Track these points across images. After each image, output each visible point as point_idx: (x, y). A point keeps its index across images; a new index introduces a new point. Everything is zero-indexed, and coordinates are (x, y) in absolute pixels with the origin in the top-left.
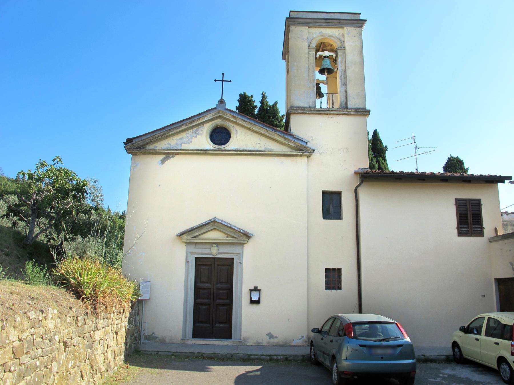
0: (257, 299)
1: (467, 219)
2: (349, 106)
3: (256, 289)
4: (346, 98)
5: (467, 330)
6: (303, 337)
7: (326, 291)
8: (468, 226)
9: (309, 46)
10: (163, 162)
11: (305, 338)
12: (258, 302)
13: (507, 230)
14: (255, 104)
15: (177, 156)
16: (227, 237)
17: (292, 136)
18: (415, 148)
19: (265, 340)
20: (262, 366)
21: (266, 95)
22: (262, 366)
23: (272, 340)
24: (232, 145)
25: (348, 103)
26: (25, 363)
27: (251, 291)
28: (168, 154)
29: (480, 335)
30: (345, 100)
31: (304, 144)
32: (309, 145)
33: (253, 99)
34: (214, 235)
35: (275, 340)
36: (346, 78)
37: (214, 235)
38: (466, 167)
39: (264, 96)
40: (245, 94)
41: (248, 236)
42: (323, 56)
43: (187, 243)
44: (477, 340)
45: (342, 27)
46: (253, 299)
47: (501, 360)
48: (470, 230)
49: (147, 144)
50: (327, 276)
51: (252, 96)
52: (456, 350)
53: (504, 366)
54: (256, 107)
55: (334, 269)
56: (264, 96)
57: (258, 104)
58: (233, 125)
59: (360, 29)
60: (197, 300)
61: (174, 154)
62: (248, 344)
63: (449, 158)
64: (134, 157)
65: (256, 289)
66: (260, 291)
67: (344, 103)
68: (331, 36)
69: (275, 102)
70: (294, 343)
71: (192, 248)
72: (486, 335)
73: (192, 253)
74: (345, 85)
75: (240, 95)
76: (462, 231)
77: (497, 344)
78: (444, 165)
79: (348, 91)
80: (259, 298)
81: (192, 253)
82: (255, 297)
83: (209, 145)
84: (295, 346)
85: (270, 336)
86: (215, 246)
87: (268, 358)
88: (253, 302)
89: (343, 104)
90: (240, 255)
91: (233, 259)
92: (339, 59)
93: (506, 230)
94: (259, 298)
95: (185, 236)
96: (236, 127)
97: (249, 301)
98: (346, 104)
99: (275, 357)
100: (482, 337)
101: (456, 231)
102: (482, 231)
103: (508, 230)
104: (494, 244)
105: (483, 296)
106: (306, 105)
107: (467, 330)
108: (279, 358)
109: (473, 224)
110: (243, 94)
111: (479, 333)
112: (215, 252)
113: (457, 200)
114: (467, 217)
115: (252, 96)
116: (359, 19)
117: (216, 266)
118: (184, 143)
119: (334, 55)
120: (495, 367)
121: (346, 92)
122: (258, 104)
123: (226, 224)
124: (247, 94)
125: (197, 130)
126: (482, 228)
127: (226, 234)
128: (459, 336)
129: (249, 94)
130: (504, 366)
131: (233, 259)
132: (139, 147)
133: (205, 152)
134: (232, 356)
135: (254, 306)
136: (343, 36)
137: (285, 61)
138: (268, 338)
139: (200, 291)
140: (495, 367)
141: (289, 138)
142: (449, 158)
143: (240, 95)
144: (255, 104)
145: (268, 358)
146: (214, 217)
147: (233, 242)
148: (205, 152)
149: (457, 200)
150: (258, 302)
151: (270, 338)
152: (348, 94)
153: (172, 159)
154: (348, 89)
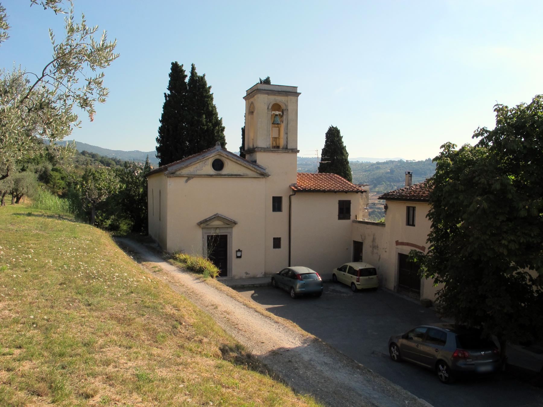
0: (240, 255)
2: (289, 147)
3: (239, 251)
4: (287, 142)
5: (340, 269)
6: (262, 273)
7: (275, 249)
9: (268, 108)
10: (187, 181)
11: (263, 273)
12: (240, 257)
14: (185, 74)
15: (194, 178)
16: (224, 224)
17: (258, 166)
18: (317, 150)
19: (244, 276)
21: (195, 66)
23: (247, 275)
24: (225, 171)
25: (288, 145)
27: (237, 251)
28: (189, 177)
29: (345, 272)
30: (286, 143)
31: (264, 171)
32: (267, 171)
33: (184, 68)
34: (217, 223)
35: (249, 275)
36: (287, 129)
37: (217, 223)
38: (341, 135)
39: (193, 68)
40: (176, 62)
41: (235, 223)
43: (202, 228)
44: (344, 274)
45: (287, 96)
46: (238, 255)
47: (353, 283)
49: (177, 171)
50: (274, 242)
51: (182, 65)
52: (335, 277)
53: (353, 286)
54: (186, 76)
55: (277, 238)
56: (193, 68)
57: (188, 73)
58: (226, 159)
59: (297, 97)
61: (193, 178)
62: (236, 278)
63: (330, 127)
65: (239, 251)
66: (241, 251)
67: (285, 145)
68: (280, 102)
69: (203, 75)
70: (258, 276)
72: (348, 273)
73: (205, 233)
74: (287, 134)
75: (172, 64)
77: (352, 277)
78: (326, 132)
79: (288, 138)
80: (241, 255)
81: (205, 233)
82: (239, 254)
83: (212, 171)
84: (259, 278)
85: (247, 273)
87: (252, 286)
88: (238, 257)
89: (285, 146)
90: (231, 233)
92: (284, 117)
94: (241, 255)
95: (202, 225)
96: (228, 160)
97: (236, 257)
98: (287, 146)
99: (255, 285)
100: (346, 274)
101: (337, 217)
102: (350, 217)
104: (354, 224)
105: (347, 249)
106: (265, 147)
107: (340, 269)
108: (257, 285)
110: (174, 62)
111: (345, 271)
112: (219, 232)
113: (339, 201)
115: (182, 65)
116: (295, 91)
118: (199, 170)
119: (281, 114)
120: (350, 285)
121: (287, 138)
122: (188, 73)
123: (223, 217)
124: (178, 63)
125: (205, 162)
126: (350, 215)
127: (224, 222)
128: (335, 271)
129: (180, 64)
130: (353, 286)
132: (173, 173)
133: (211, 176)
134: (236, 286)
135: (238, 259)
136: (287, 102)
138: (245, 274)
140: (350, 285)
141: (256, 167)
142: (330, 127)
143: (172, 64)
144: (185, 74)
145: (252, 286)
146: (216, 213)
147: (227, 226)
148: (211, 176)
149: (339, 201)
150: (240, 257)
151: (246, 274)
152: (288, 140)
153: (192, 180)
154: (288, 136)
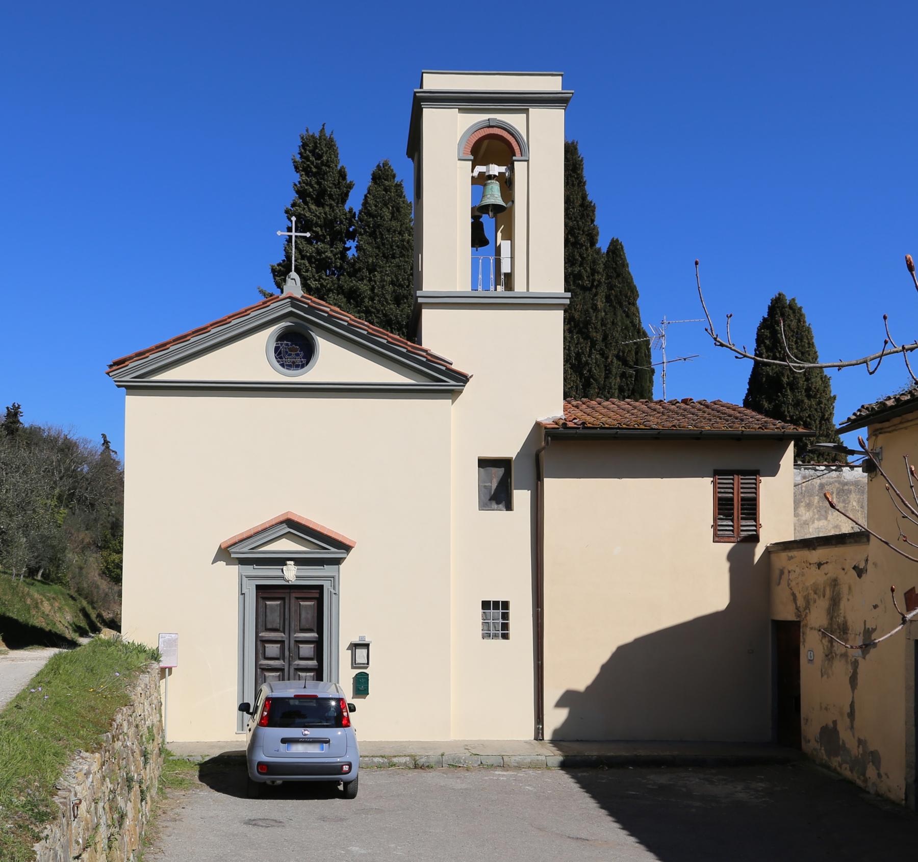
1: (733, 509)
8: (733, 522)
13: (848, 503)
20: (793, 443)
22: (793, 443)
26: (170, 798)
42: (487, 174)
48: (736, 530)
60: (260, 635)
64: (128, 390)
71: (250, 570)
73: (249, 577)
76: (721, 533)
82: (361, 654)
86: (291, 565)
90: (333, 579)
91: (322, 586)
93: (847, 502)
103: (850, 502)
109: (743, 519)
114: (733, 505)
117: (292, 642)
131: (322, 586)
137: (413, 161)
139: (267, 602)
